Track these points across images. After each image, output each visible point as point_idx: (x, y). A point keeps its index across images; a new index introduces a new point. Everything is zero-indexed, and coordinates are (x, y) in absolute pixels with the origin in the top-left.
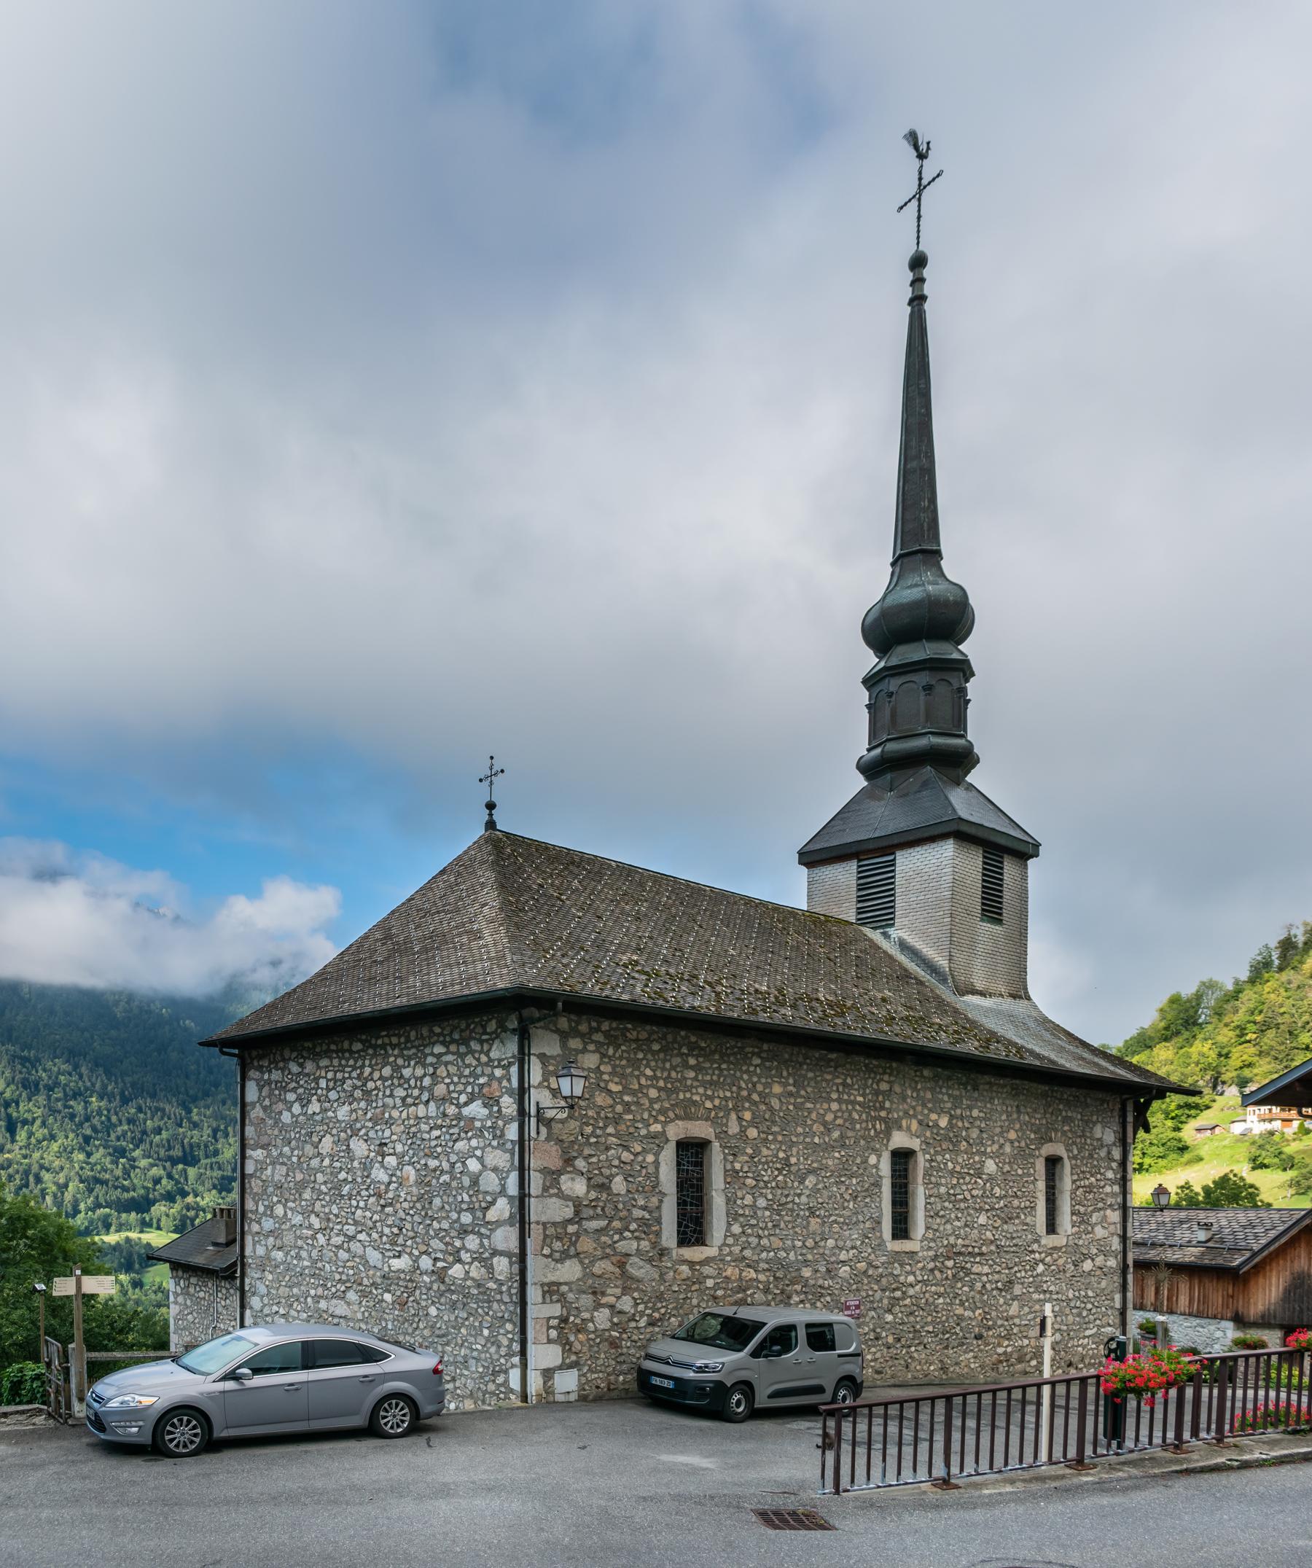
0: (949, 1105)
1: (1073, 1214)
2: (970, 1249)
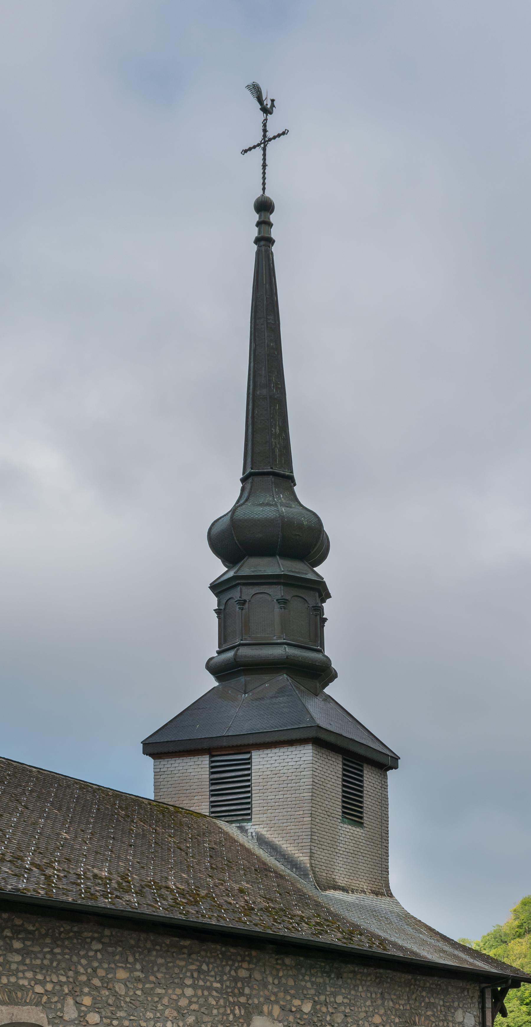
0: (312, 992)
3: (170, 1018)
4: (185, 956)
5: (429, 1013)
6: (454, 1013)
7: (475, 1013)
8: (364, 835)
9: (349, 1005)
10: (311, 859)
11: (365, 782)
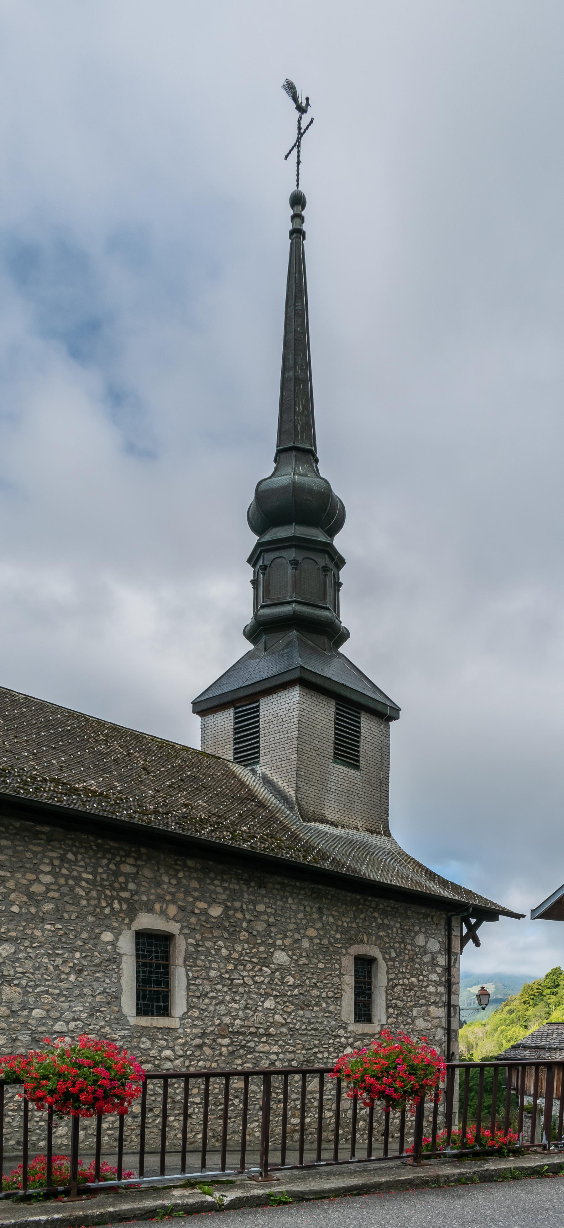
0: (224, 897)
1: (388, 1007)
2: (252, 1030)
3: (17, 903)
4: (42, 842)
5: (381, 934)
6: (414, 937)
7: (440, 939)
8: (359, 777)
9: (273, 915)
10: (296, 793)
11: (362, 728)
